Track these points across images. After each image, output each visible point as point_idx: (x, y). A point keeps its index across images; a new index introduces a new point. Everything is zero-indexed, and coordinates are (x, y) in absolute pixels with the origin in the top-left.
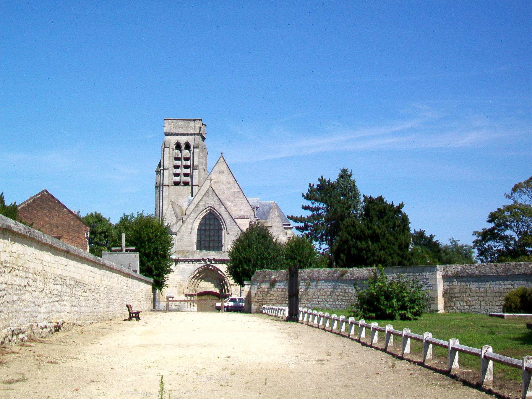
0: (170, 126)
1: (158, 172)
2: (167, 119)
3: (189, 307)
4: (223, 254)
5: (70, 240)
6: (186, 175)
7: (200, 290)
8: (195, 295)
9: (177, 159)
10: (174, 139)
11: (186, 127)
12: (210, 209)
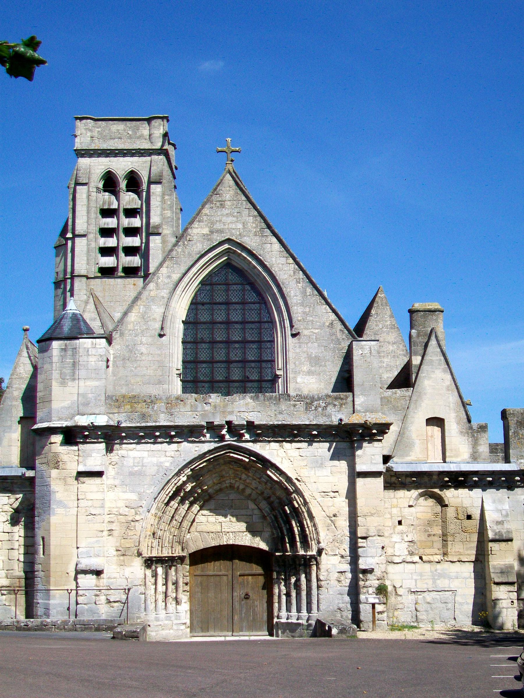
0: (89, 134)
1: (60, 248)
2: (81, 119)
3: (161, 604)
4: (283, 406)
5: (245, 624)
6: (130, 251)
7: (197, 542)
8: (182, 559)
9: (107, 213)
10: (98, 166)
11: (130, 137)
12: (227, 252)
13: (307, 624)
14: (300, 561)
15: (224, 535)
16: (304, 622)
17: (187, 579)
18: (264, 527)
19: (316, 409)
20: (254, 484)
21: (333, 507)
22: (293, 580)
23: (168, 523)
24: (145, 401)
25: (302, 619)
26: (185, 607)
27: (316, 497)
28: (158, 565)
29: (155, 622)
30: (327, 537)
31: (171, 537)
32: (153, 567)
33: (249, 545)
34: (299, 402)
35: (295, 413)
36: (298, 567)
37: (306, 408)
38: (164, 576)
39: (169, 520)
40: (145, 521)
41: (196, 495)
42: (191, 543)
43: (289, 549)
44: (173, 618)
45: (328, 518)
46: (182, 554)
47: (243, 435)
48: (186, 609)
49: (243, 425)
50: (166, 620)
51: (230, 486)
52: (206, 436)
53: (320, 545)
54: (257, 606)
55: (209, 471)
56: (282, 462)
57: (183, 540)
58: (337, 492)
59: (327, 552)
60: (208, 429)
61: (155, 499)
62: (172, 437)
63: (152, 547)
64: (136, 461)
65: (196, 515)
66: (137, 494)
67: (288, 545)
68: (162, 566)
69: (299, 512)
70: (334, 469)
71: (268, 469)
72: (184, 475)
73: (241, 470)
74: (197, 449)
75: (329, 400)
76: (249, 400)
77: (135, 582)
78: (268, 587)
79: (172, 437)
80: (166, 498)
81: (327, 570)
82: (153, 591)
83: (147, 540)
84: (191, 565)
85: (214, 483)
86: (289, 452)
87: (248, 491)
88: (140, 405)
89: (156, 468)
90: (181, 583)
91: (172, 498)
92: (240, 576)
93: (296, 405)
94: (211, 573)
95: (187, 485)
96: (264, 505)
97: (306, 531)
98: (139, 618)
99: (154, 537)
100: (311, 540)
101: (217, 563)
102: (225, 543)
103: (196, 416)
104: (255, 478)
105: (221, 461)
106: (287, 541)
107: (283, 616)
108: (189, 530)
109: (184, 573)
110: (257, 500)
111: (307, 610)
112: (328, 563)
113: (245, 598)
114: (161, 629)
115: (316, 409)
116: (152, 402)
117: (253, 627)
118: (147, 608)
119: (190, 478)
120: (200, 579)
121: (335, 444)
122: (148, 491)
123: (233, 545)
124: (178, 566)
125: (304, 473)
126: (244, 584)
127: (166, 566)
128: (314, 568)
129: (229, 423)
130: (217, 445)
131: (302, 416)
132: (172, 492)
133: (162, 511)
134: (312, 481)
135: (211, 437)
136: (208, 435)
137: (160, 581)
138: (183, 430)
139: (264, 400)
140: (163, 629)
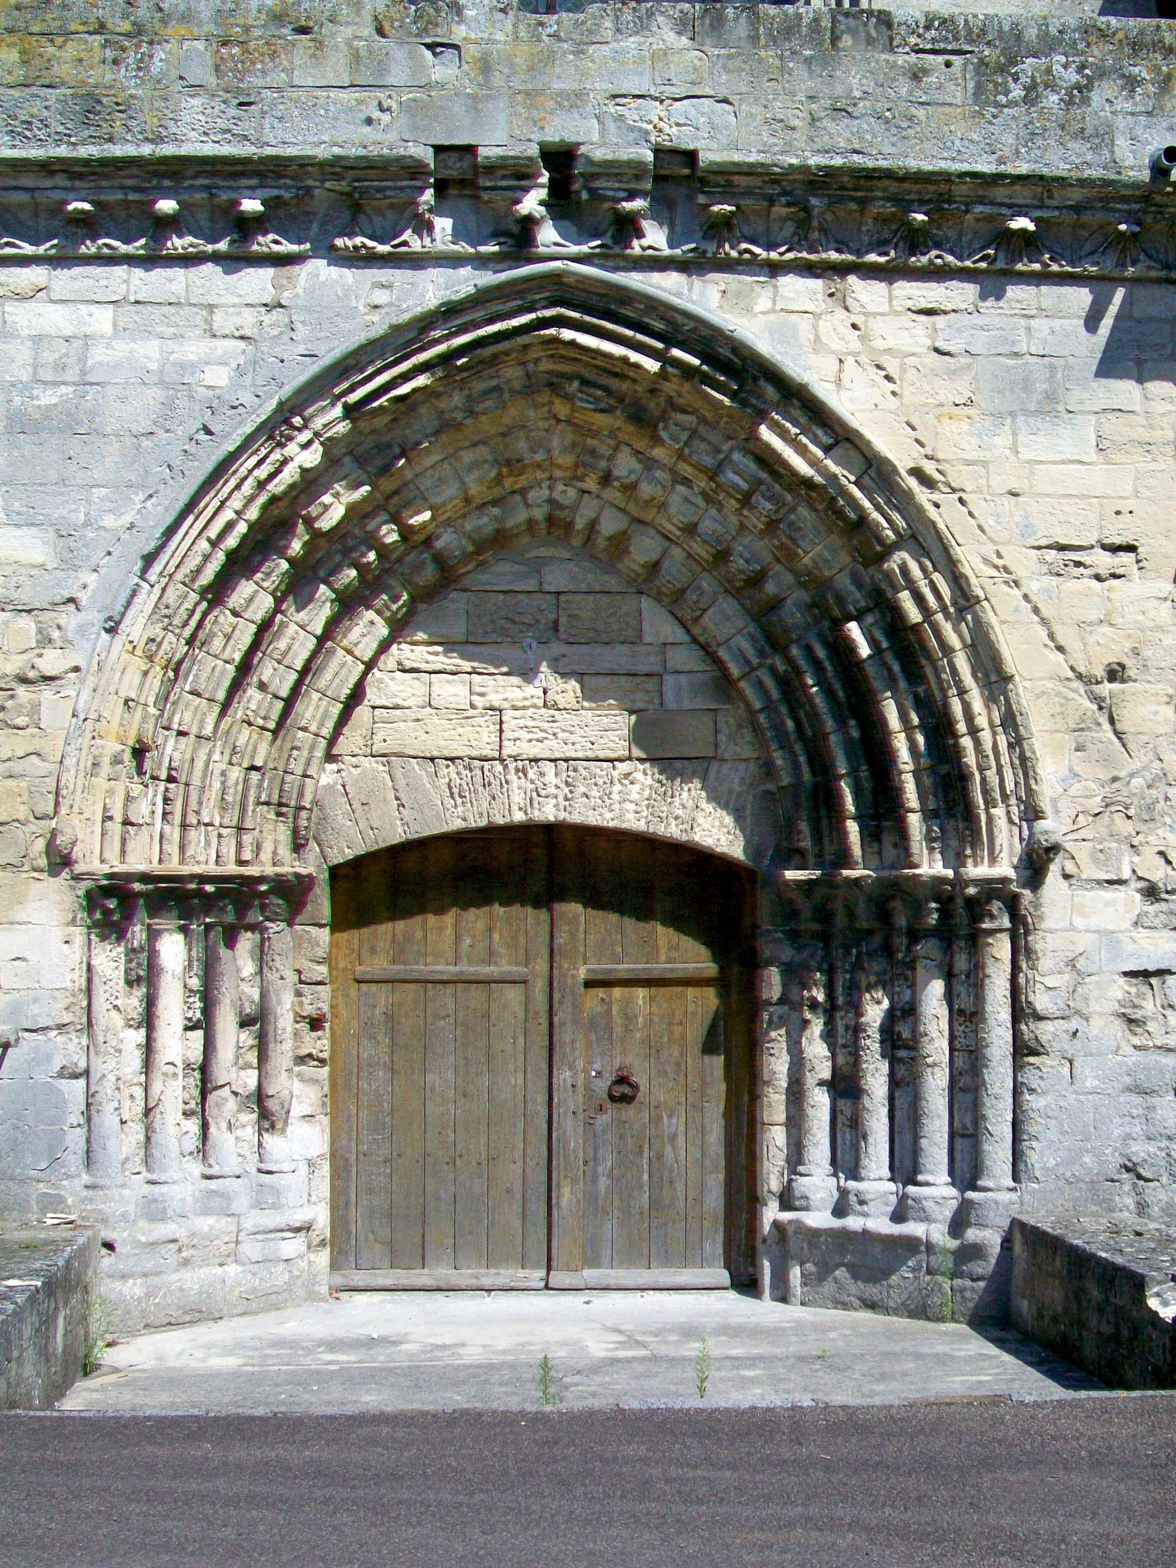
3: (175, 1129)
4: (855, 75)
7: (372, 805)
8: (291, 894)
13: (953, 1244)
14: (917, 908)
15: (512, 777)
16: (938, 1233)
17: (320, 1000)
18: (722, 738)
19: (1031, 97)
20: (680, 506)
21: (1105, 629)
22: (875, 1011)
23: (221, 695)
24: (101, 28)
25: (927, 1219)
26: (305, 1140)
27: (1020, 572)
28: (159, 923)
29: (142, 1223)
30: (1076, 788)
31: (236, 774)
32: (137, 933)
33: (640, 826)
34: (940, 59)
35: (921, 113)
36: (901, 942)
37: (979, 90)
38: (195, 983)
39: (227, 683)
40: (91, 682)
41: (372, 556)
42: (339, 813)
43: (857, 850)
44: (242, 1203)
45: (1077, 685)
46: (290, 866)
47: (628, 227)
48: (314, 1153)
49: (636, 169)
50: (206, 1212)
51: (550, 520)
52: (430, 227)
53: (1041, 825)
54: (673, 1138)
55: (447, 425)
56: (838, 382)
57: (301, 795)
58: (1131, 548)
59: (1070, 868)
60: (441, 187)
61: (149, 560)
62: (246, 227)
63: (127, 822)
64: (48, 357)
65: (370, 665)
66: (52, 536)
67: (852, 827)
68: (184, 930)
69: (925, 650)
70: (1114, 426)
71: (762, 416)
72: (306, 436)
73: (613, 433)
74: (381, 297)
75: (1098, 53)
76: (671, 37)
77: (35, 1009)
78: (736, 1038)
79: (246, 227)
80: (207, 558)
81: (1072, 963)
82: (133, 1060)
83: (101, 782)
84: (338, 924)
85: (467, 500)
86: (877, 327)
87: (644, 549)
88: (72, 49)
89: (158, 394)
90: (284, 1021)
91: (241, 563)
92: (589, 984)
93: (926, 72)
94: (443, 969)
95: (327, 499)
96: (727, 623)
97: (958, 751)
98: (53, 1203)
99: (140, 772)
100: (990, 803)
101: (476, 918)
102: (519, 817)
103: (376, 114)
104: (686, 469)
105: (512, 373)
106: (850, 805)
107: (816, 1197)
108: (332, 741)
109: (305, 964)
110: (692, 596)
111: (951, 1172)
112: (1079, 922)
113: (612, 1098)
114: (173, 1260)
115: (1031, 97)
116: (138, 31)
117: (648, 1241)
118: (98, 1155)
119: (338, 460)
120: (382, 997)
121: (1120, 293)
122: (109, 521)
123: (551, 832)
124: (273, 927)
125: (957, 443)
126: (609, 1028)
127: (209, 928)
128: (1001, 948)
129: (560, 158)
130: (488, 278)
131: (959, 129)
132: (242, 528)
133: (187, 632)
134: (1001, 482)
135: (458, 235)
136: (443, 225)
137: (174, 1006)
138: (308, 190)
139: (754, 39)
140: (186, 1262)
